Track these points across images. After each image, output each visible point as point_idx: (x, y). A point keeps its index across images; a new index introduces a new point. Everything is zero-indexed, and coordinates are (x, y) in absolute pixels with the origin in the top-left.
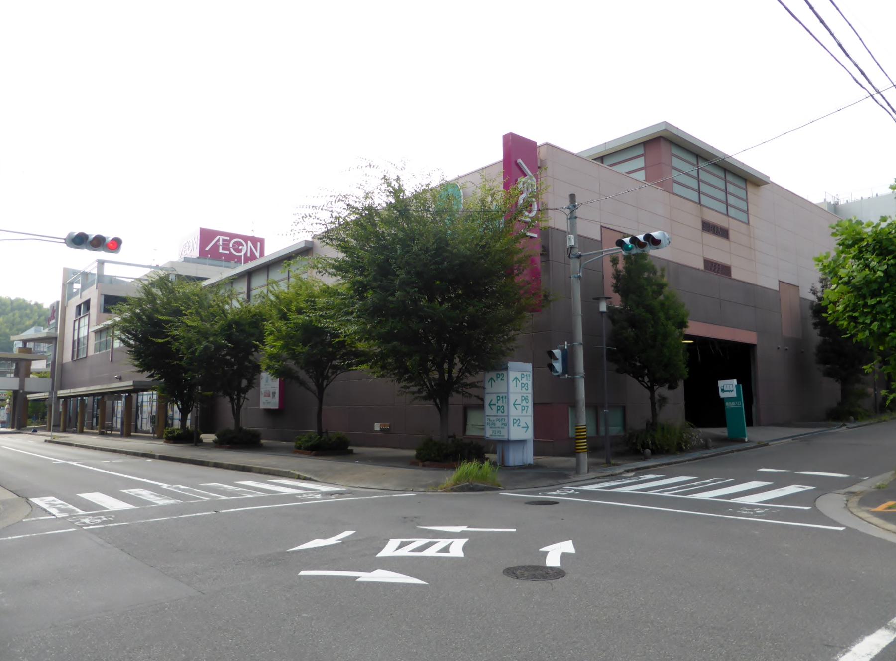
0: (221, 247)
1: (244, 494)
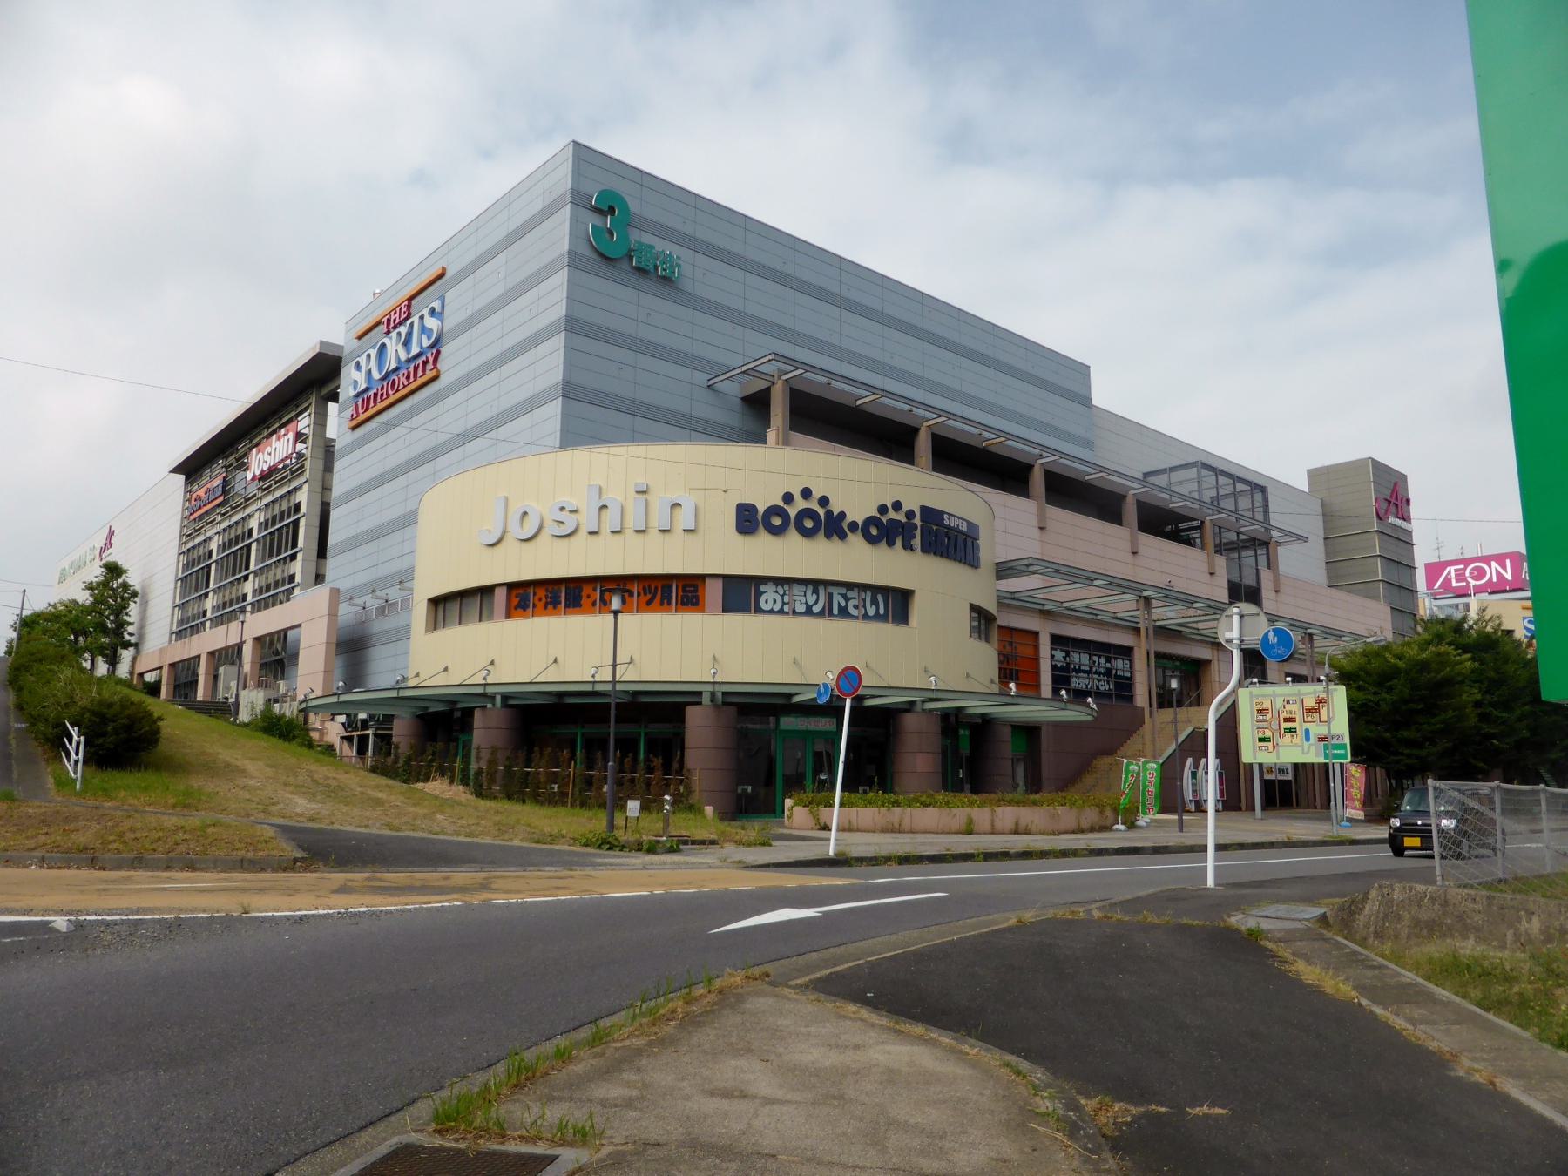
0: (1454, 581)
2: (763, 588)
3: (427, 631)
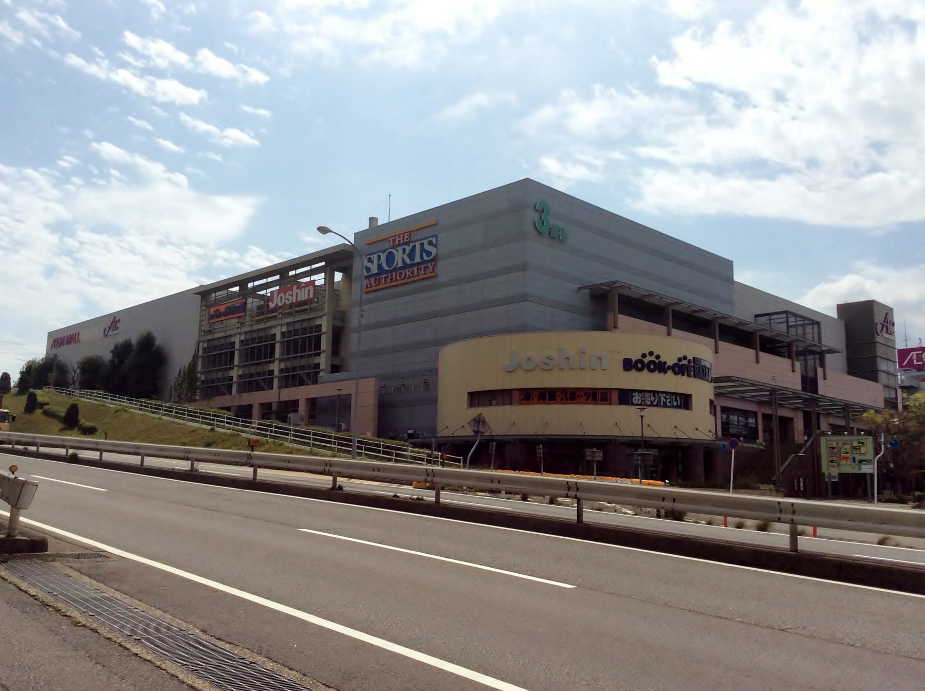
0: (915, 361)
1: (700, 521)
2: (634, 394)
3: (467, 408)
